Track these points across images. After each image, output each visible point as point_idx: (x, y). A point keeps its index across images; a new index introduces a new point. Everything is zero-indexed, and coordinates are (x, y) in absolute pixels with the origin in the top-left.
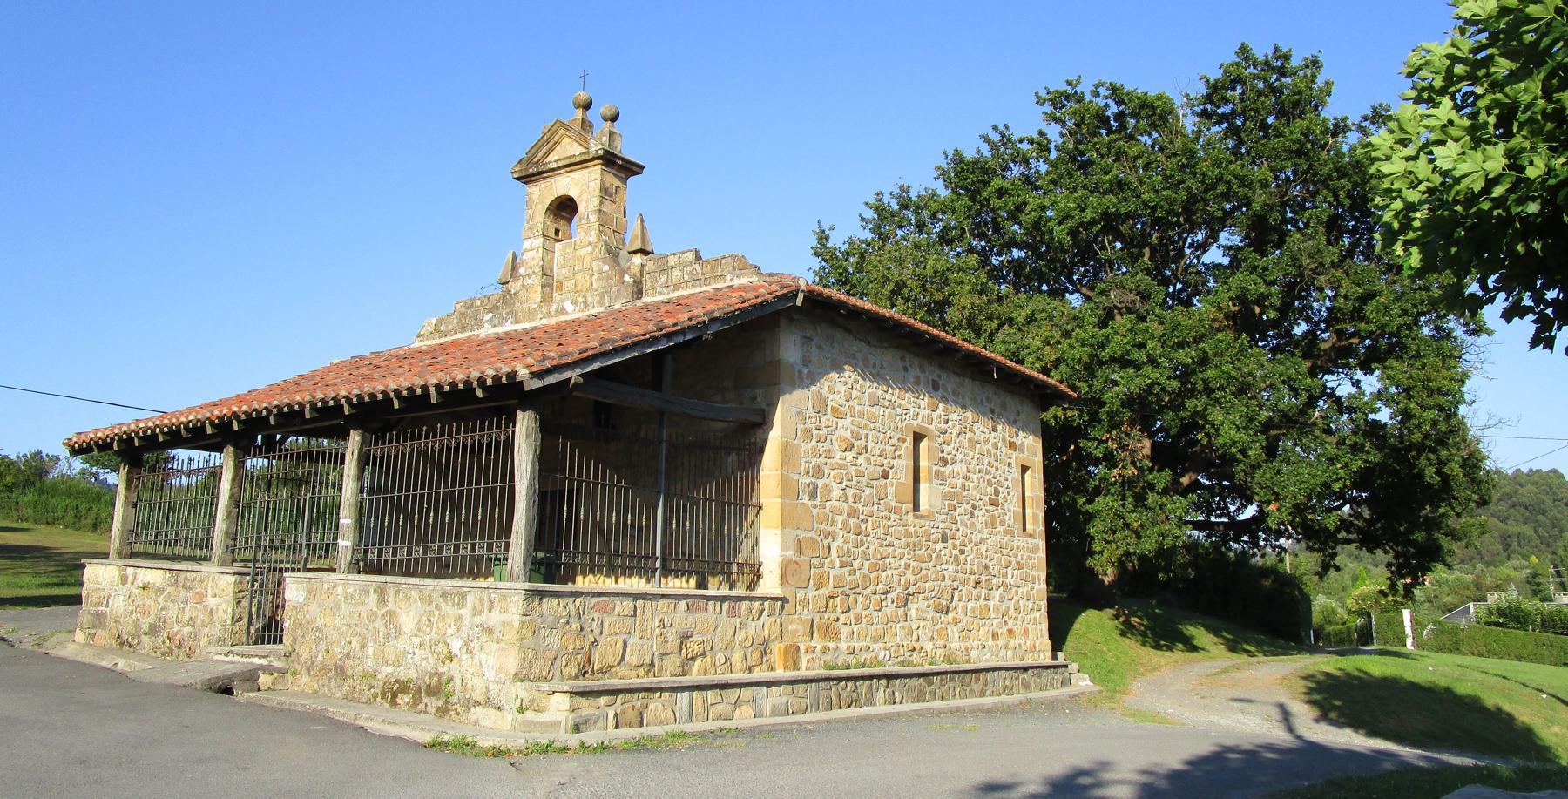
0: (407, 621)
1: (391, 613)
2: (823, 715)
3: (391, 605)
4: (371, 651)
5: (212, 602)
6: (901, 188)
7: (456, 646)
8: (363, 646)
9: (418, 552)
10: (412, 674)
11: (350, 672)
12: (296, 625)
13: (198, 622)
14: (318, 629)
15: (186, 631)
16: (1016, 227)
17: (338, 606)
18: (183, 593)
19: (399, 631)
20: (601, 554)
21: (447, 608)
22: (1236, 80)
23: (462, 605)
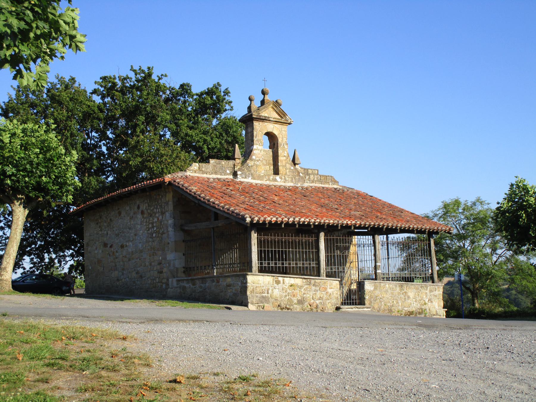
0: (411, 294)
1: (406, 292)
2: (89, 325)
3: (405, 290)
4: (400, 304)
5: (330, 291)
6: (149, 68)
7: (427, 301)
8: (397, 303)
9: (272, 264)
10: (414, 309)
11: (393, 311)
12: (371, 297)
13: (324, 298)
14: (381, 298)
15: (318, 302)
16: (244, 132)
17: (388, 291)
18: (313, 288)
19: (409, 297)
20: (235, 263)
21: (423, 291)
22: (514, 192)
23: (427, 289)
